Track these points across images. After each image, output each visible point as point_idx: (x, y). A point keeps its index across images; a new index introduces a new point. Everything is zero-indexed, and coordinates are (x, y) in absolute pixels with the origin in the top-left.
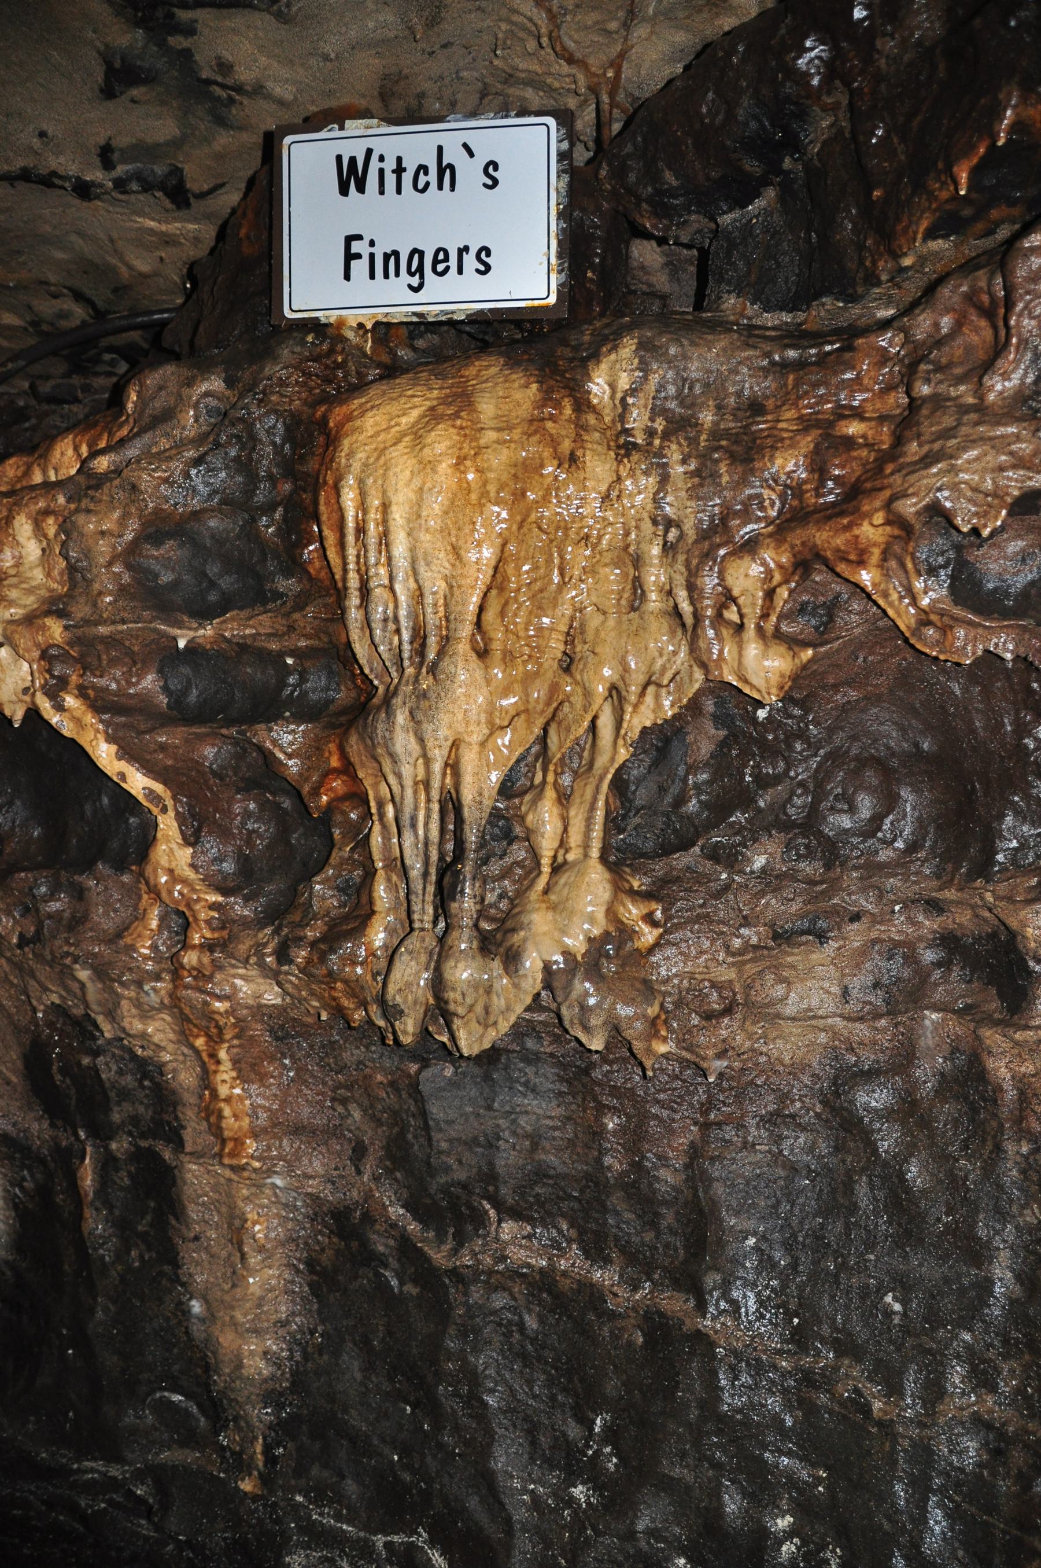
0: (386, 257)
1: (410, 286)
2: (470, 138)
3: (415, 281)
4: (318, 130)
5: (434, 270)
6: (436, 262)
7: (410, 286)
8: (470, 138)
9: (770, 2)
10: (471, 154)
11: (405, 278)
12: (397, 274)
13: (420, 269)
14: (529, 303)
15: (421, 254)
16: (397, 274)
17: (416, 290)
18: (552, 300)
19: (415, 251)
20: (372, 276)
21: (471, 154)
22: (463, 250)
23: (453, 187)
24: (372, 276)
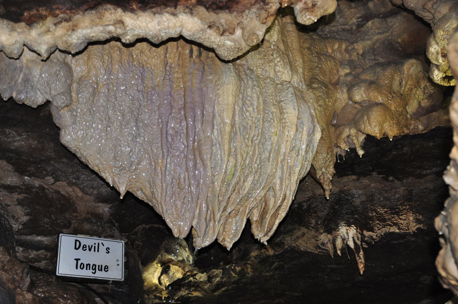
0: (87, 265)
1: (92, 272)
2: (104, 242)
3: (94, 271)
4: (77, 235)
5: (105, 270)
6: (105, 268)
7: (92, 272)
8: (104, 242)
9: (1, 248)
10: (103, 245)
11: (91, 270)
12: (89, 269)
13: (95, 269)
14: (94, 278)
15: (96, 266)
16: (89, 269)
17: (94, 273)
18: (123, 280)
19: (82, 264)
20: (77, 268)
21: (103, 245)
22: (87, 265)
23: (98, 251)
24: (77, 268)
